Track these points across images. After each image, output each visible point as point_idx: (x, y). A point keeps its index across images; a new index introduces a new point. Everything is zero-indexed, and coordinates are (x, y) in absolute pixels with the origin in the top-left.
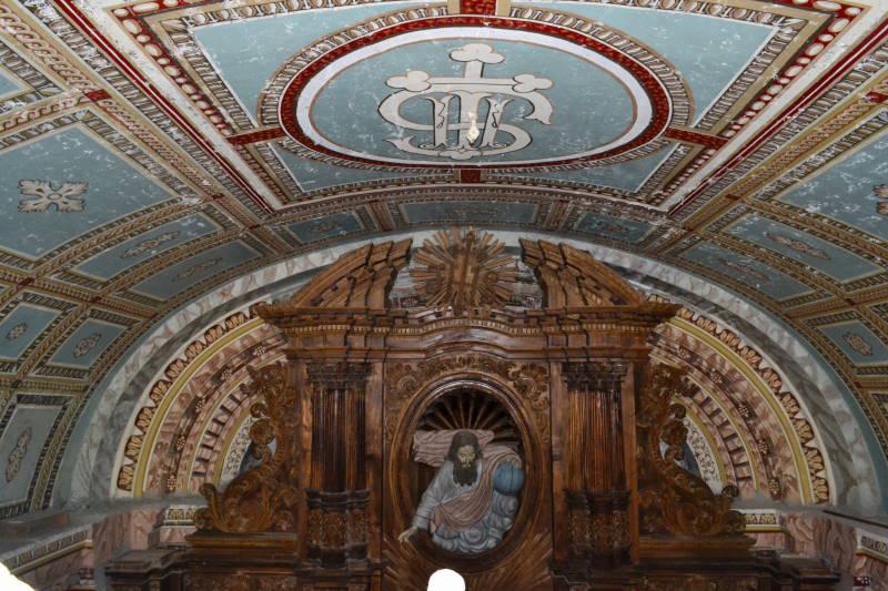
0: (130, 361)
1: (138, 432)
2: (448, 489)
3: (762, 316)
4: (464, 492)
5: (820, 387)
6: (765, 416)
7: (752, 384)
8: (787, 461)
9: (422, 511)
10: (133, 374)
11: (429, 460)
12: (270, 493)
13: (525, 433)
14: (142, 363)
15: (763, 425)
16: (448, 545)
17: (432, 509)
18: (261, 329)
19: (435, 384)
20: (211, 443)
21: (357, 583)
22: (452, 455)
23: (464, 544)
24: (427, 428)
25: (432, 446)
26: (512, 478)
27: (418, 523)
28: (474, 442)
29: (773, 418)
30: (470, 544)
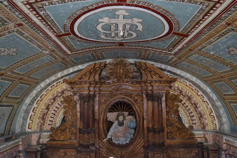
0: (31, 95)
1: (33, 114)
2: (116, 128)
3: (199, 81)
4: (121, 128)
5: (214, 99)
6: (200, 107)
7: (196, 99)
8: (205, 119)
9: (110, 134)
10: (32, 98)
11: (111, 120)
12: (69, 129)
13: (136, 112)
14: (34, 95)
15: (199, 109)
16: (116, 142)
17: (112, 133)
18: (66, 86)
19: (113, 100)
20: (53, 116)
21: (92, 153)
22: (117, 119)
23: (121, 142)
24: (111, 112)
25: (112, 116)
26: (133, 125)
27: (109, 137)
28: (123, 115)
29: (202, 108)
30: (122, 142)
